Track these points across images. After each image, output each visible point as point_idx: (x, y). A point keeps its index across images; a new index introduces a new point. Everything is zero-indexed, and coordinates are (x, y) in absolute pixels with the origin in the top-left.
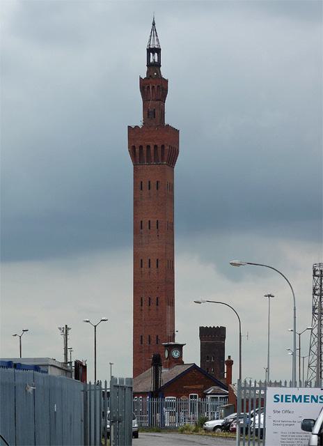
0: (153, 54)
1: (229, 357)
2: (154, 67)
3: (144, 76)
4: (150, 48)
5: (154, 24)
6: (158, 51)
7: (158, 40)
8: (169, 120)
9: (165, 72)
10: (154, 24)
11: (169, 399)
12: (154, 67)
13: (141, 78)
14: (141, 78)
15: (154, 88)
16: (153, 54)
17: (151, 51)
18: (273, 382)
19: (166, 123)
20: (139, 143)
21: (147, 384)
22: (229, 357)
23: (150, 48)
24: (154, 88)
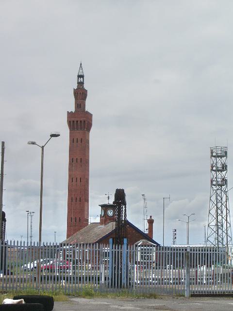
2: (81, 84)
5: (81, 64)
6: (82, 76)
8: (88, 108)
9: (86, 87)
10: (81, 64)
12: (81, 84)
15: (80, 94)
24: (80, 94)
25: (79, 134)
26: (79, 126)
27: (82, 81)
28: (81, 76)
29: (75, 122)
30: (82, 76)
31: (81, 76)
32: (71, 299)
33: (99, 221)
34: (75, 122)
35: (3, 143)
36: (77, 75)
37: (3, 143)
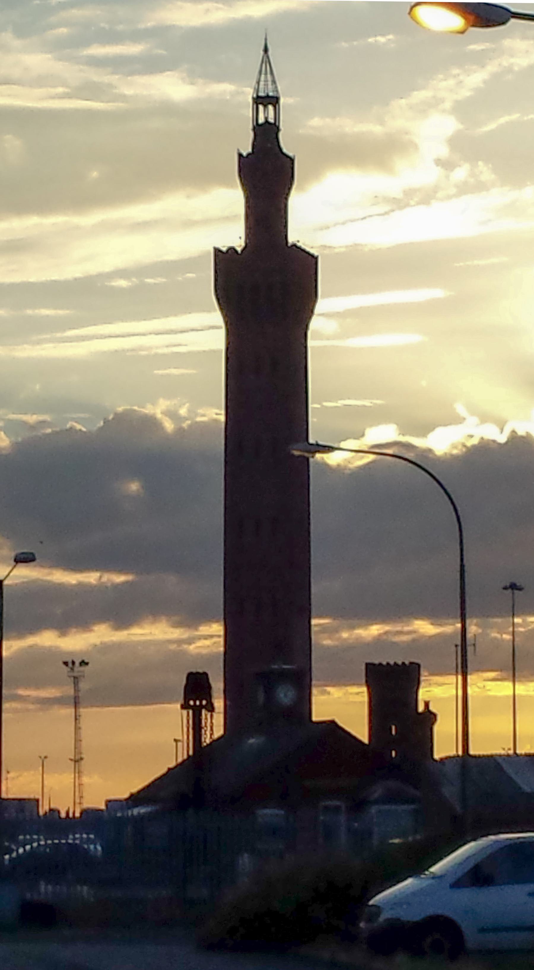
0: (265, 106)
1: (427, 704)
3: (247, 149)
4: (258, 97)
5: (266, 50)
6: (274, 101)
7: (274, 82)
10: (266, 50)
11: (269, 814)
13: (240, 155)
14: (240, 155)
16: (267, 121)
17: (260, 101)
18: (400, 196)
19: (291, 239)
20: (446, 761)
21: (69, 670)
22: (427, 704)
23: (258, 97)
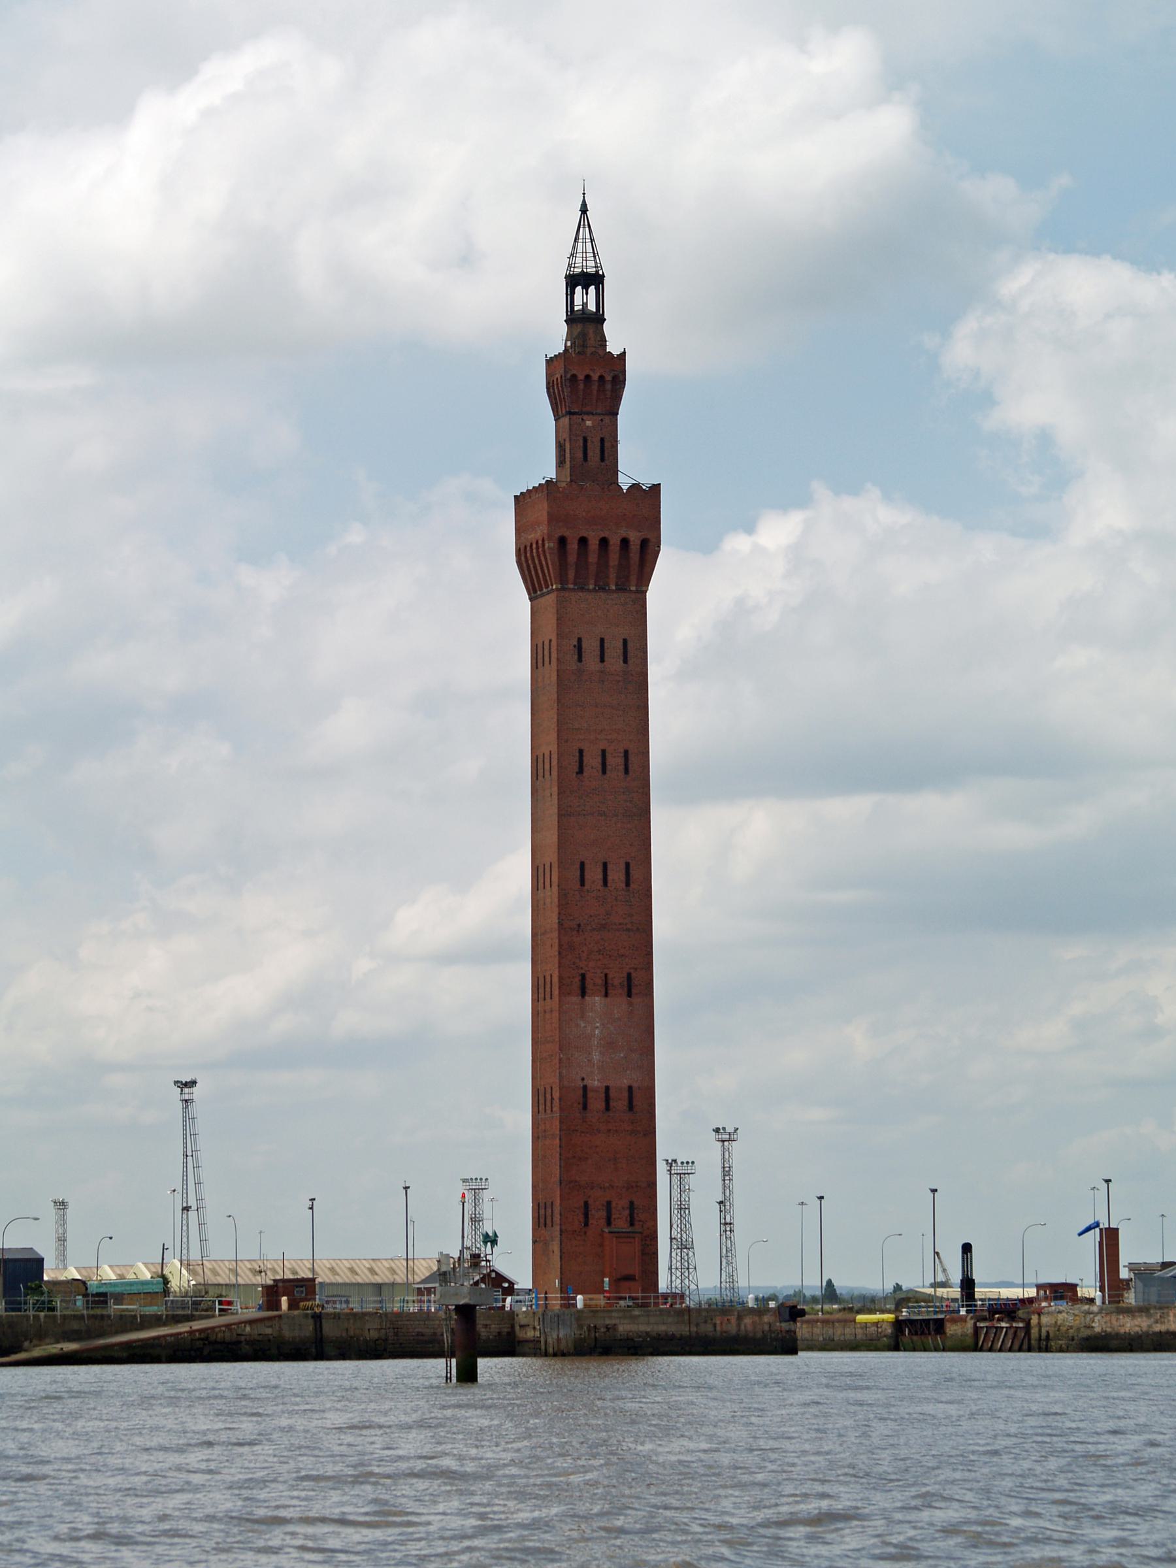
2: (586, 325)
5: (584, 210)
6: (595, 280)
8: (633, 466)
10: (584, 210)
12: (586, 325)
25: (596, 612)
26: (613, 575)
27: (592, 307)
28: (585, 280)
29: (573, 546)
30: (595, 280)
31: (585, 280)
32: (564, 1508)
33: (958, 1296)
34: (573, 546)
35: (1080, 1234)
36: (563, 272)
37: (1080, 1234)
